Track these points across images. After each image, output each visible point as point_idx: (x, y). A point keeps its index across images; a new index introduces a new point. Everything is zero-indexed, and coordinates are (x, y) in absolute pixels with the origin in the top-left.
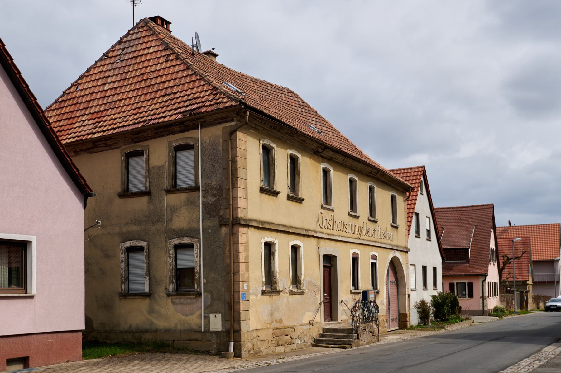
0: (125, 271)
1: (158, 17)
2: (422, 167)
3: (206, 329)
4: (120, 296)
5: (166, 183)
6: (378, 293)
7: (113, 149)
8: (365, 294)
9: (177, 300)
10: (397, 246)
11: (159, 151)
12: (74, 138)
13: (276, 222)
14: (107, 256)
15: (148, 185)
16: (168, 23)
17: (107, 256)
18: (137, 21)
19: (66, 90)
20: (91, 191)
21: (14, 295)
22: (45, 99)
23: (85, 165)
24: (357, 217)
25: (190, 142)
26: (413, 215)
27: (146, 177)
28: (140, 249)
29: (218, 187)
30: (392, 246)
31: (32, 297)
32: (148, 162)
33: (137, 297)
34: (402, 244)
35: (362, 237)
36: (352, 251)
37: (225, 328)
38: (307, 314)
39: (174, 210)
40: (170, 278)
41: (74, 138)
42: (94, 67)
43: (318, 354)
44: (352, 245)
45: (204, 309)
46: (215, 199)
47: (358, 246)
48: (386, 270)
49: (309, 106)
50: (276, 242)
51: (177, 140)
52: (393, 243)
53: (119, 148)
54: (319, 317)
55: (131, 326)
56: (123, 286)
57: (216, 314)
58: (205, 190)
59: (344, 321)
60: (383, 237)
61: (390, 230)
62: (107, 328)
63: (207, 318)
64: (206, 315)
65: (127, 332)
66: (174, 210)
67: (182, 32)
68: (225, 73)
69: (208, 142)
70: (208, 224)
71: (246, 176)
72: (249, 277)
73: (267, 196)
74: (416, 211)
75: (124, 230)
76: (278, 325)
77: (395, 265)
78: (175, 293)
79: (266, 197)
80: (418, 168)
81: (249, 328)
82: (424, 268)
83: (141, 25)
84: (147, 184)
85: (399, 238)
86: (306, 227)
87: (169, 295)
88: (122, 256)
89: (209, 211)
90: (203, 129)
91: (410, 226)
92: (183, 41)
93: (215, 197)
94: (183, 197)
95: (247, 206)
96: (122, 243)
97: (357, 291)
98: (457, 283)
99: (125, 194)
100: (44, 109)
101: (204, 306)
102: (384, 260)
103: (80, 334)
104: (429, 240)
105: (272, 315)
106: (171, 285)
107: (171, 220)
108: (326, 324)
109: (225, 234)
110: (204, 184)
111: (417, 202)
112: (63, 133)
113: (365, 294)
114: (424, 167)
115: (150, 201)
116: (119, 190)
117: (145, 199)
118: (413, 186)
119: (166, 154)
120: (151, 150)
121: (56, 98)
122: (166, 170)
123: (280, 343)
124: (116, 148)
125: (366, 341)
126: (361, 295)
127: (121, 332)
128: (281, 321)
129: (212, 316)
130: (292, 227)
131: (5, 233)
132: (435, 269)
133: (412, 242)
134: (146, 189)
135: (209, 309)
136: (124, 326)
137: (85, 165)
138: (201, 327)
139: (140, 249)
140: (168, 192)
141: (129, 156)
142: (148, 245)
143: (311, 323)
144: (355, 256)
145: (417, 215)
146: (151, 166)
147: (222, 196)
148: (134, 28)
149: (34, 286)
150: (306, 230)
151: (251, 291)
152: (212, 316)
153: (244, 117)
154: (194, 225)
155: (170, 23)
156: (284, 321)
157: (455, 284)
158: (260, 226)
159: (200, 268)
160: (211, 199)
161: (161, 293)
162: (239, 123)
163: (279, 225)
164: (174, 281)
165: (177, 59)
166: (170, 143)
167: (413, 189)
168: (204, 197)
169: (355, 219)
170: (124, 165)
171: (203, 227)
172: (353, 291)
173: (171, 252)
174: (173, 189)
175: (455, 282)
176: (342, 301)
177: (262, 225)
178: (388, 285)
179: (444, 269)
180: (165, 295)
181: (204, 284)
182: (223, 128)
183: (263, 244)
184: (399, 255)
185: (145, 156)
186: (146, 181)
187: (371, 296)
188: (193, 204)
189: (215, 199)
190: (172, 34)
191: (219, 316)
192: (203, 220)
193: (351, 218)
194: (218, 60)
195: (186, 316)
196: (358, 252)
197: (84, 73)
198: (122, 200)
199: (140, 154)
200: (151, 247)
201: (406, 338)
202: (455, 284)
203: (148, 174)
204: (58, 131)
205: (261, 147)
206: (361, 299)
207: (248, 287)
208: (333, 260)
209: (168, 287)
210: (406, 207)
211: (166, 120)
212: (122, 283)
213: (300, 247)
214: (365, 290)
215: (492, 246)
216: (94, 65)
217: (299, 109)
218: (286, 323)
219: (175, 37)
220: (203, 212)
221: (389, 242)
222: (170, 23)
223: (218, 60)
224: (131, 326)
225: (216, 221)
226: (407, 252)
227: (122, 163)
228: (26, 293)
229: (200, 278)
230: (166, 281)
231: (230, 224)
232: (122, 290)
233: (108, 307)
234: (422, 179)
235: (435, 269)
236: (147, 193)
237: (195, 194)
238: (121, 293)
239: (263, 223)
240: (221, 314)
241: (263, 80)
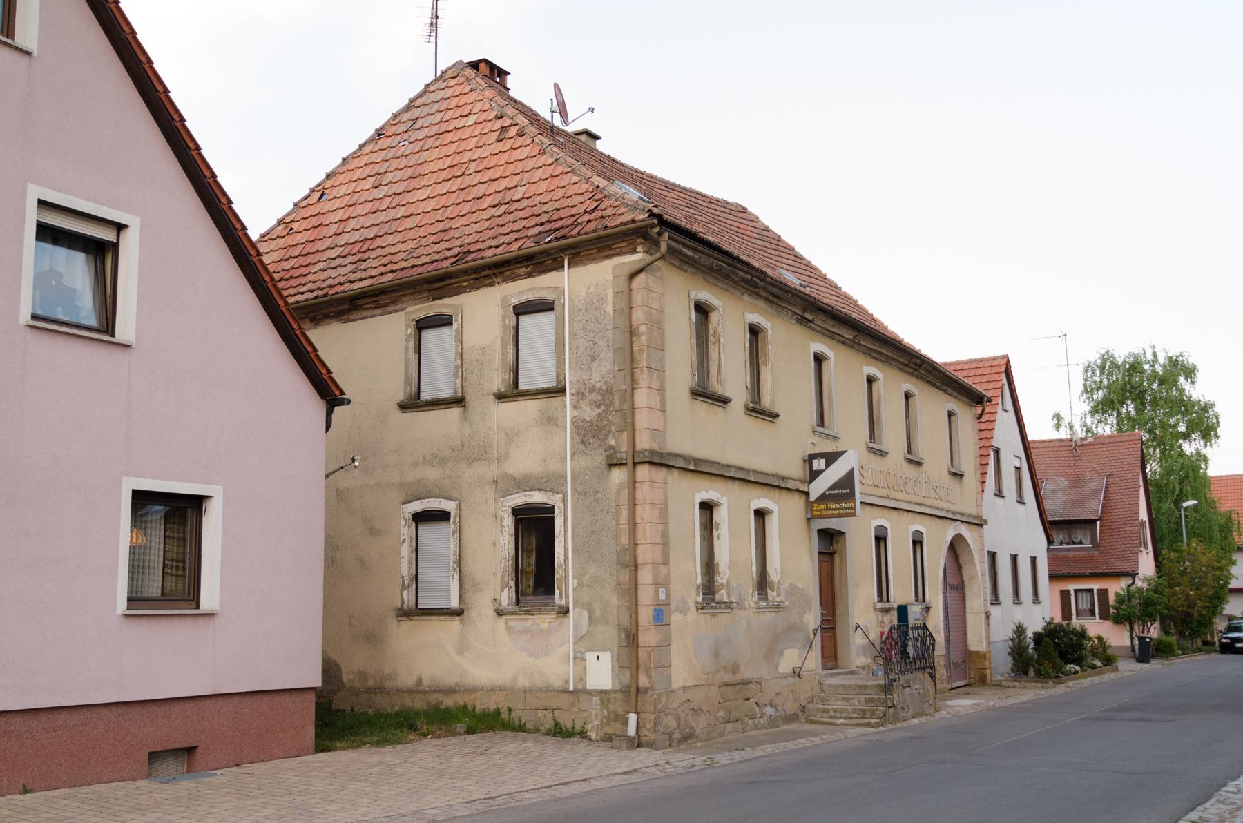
0: (410, 563)
1: (485, 61)
2: (1003, 357)
3: (579, 687)
4: (398, 615)
5: (498, 380)
6: (928, 609)
7: (391, 312)
8: (903, 611)
9: (517, 622)
10: (962, 514)
11: (482, 311)
12: (312, 291)
13: (724, 460)
14: (373, 532)
15: (459, 385)
16: (503, 73)
17: (373, 532)
18: (442, 66)
19: (300, 201)
20: (342, 393)
21: (169, 612)
22: (258, 216)
23: (328, 340)
24: (883, 454)
25: (546, 295)
26: (990, 452)
27: (456, 367)
28: (443, 516)
29: (604, 388)
30: (953, 513)
31: (210, 615)
32: (459, 339)
33: (434, 618)
34: (971, 509)
35: (893, 494)
36: (875, 523)
37: (620, 682)
38: (788, 652)
39: (511, 436)
40: (503, 576)
41: (312, 291)
42: (355, 155)
43: (817, 740)
44: (875, 511)
45: (575, 644)
46: (597, 411)
47: (886, 511)
48: (942, 563)
49: (779, 239)
50: (724, 501)
51: (521, 293)
52: (953, 508)
53: (402, 310)
54: (813, 661)
55: (419, 681)
56: (405, 593)
57: (601, 654)
58: (578, 393)
59: (863, 668)
60: (933, 495)
61: (947, 479)
62: (370, 683)
63: (580, 659)
64: (579, 655)
65: (410, 691)
66: (511, 436)
67: (530, 88)
68: (613, 168)
69: (584, 294)
70: (583, 463)
71: (663, 366)
72: (669, 574)
73: (704, 406)
74: (995, 443)
75: (410, 477)
76: (728, 677)
77: (956, 548)
78: (511, 608)
79: (702, 407)
80: (994, 358)
81: (670, 682)
82: (1014, 558)
83: (449, 74)
84: (459, 382)
85: (964, 499)
86: (784, 473)
87: (499, 613)
88: (406, 531)
89: (587, 434)
90: (574, 270)
91: (984, 474)
92: (533, 108)
93: (599, 407)
94: (532, 407)
95: (665, 425)
96: (405, 503)
97: (887, 605)
98: (1076, 591)
99: (413, 403)
100: (254, 236)
101: (574, 637)
102: (938, 539)
103: (311, 698)
104: (1021, 501)
105: (716, 654)
106: (506, 590)
107: (507, 456)
108: (826, 676)
109: (620, 484)
110: (574, 380)
111: (997, 426)
112: (292, 282)
113: (903, 611)
114: (1007, 357)
115: (465, 417)
116: (401, 396)
117: (454, 413)
118: (989, 394)
119: (498, 321)
120: (467, 313)
121: (280, 216)
122: (498, 356)
123: (734, 715)
124: (395, 311)
125: (911, 712)
126: (895, 613)
127: (400, 691)
128: (735, 669)
129: (591, 657)
130: (756, 472)
131: (155, 478)
132: (1033, 560)
133: (991, 508)
134: (455, 392)
135: (585, 642)
136: (406, 679)
137: (328, 340)
138: (567, 682)
139: (442, 516)
140: (500, 397)
141: (423, 325)
142: (459, 508)
143: (797, 673)
144: (881, 534)
145: (997, 452)
146: (465, 347)
147: (612, 404)
148: (437, 80)
149: (210, 596)
150: (783, 478)
151: (673, 605)
152: (591, 657)
153: (657, 244)
154: (554, 467)
155: (508, 73)
156: (742, 668)
157: (1072, 592)
158: (692, 467)
159: (566, 556)
160: (589, 413)
161: (482, 607)
162: (649, 258)
163: (729, 466)
164: (512, 583)
165: (521, 134)
166: (505, 300)
167: (989, 400)
168: (575, 407)
169: (878, 458)
170: (412, 344)
171: (572, 470)
172: (880, 605)
173: (505, 523)
174: (512, 392)
175: (1072, 586)
176: (857, 627)
177: (696, 465)
178: (945, 593)
179: (1052, 561)
180: (491, 613)
181: (574, 589)
182: (614, 267)
183: (697, 506)
184: (965, 531)
185: (455, 326)
186: (455, 376)
187: (915, 611)
188: (550, 421)
189: (597, 411)
190: (511, 93)
191: (606, 657)
192: (573, 455)
193: (872, 455)
194: (600, 146)
195: (536, 657)
196: (923, 530)
197: (338, 167)
198: (407, 416)
199: (444, 321)
200: (465, 512)
201: (991, 703)
202: (1072, 592)
203: (459, 362)
204: (281, 279)
205: (692, 307)
206: (895, 622)
207: (657, 592)
208: (837, 541)
209: (497, 597)
210: (977, 437)
211: (498, 251)
212: (404, 587)
213: (770, 512)
214: (902, 602)
215: (1143, 515)
216: (355, 152)
217: (760, 243)
218: (746, 674)
219: (517, 98)
220: (572, 439)
221: (945, 505)
222: (508, 73)
223: (600, 146)
224: (419, 681)
225: (599, 458)
226: (982, 525)
227: (407, 341)
228: (198, 607)
229: (566, 576)
230: (496, 582)
231: (630, 464)
232: (403, 603)
233: (373, 638)
234: (1005, 381)
235: (1033, 560)
236: (458, 401)
237: (555, 401)
238: (401, 609)
239: (697, 461)
240: (609, 654)
241: (688, 186)
